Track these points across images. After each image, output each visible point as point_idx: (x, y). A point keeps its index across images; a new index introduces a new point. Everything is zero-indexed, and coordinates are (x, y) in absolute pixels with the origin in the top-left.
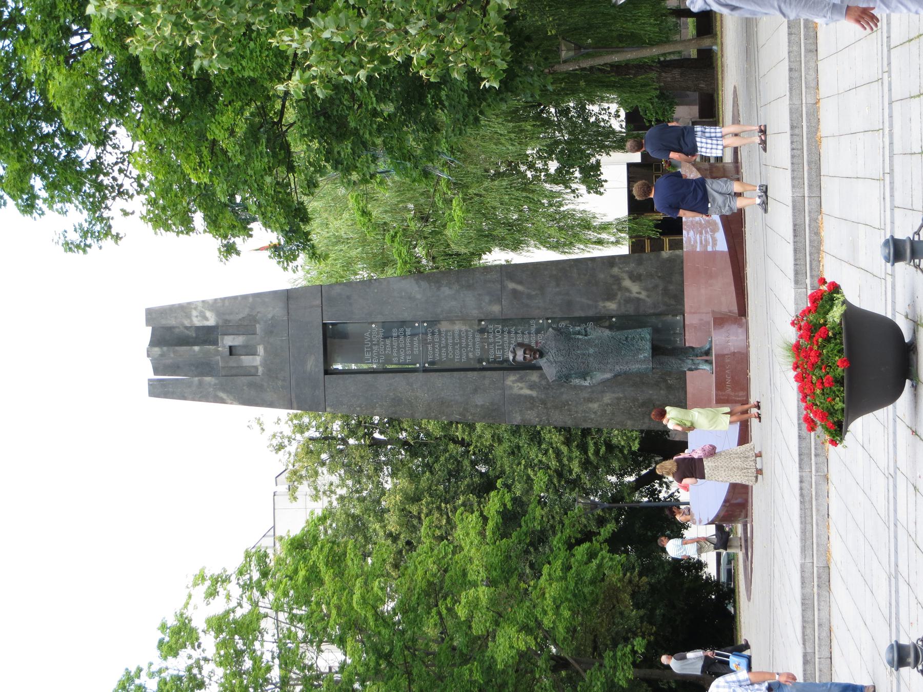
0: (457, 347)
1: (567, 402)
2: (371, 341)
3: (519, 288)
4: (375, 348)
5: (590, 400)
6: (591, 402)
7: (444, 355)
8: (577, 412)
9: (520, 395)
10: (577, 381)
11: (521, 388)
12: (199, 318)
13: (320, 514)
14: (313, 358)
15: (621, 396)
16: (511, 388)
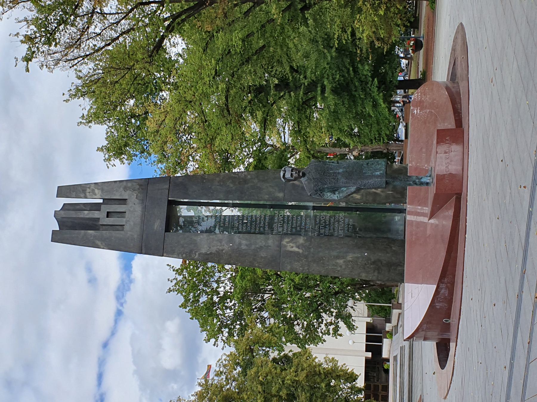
0: (254, 223)
1: (322, 258)
5: (338, 257)
6: (339, 259)
8: (328, 265)
9: (291, 252)
10: (329, 194)
11: (292, 247)
12: (91, 194)
14: (159, 221)
15: (359, 256)
16: (286, 246)
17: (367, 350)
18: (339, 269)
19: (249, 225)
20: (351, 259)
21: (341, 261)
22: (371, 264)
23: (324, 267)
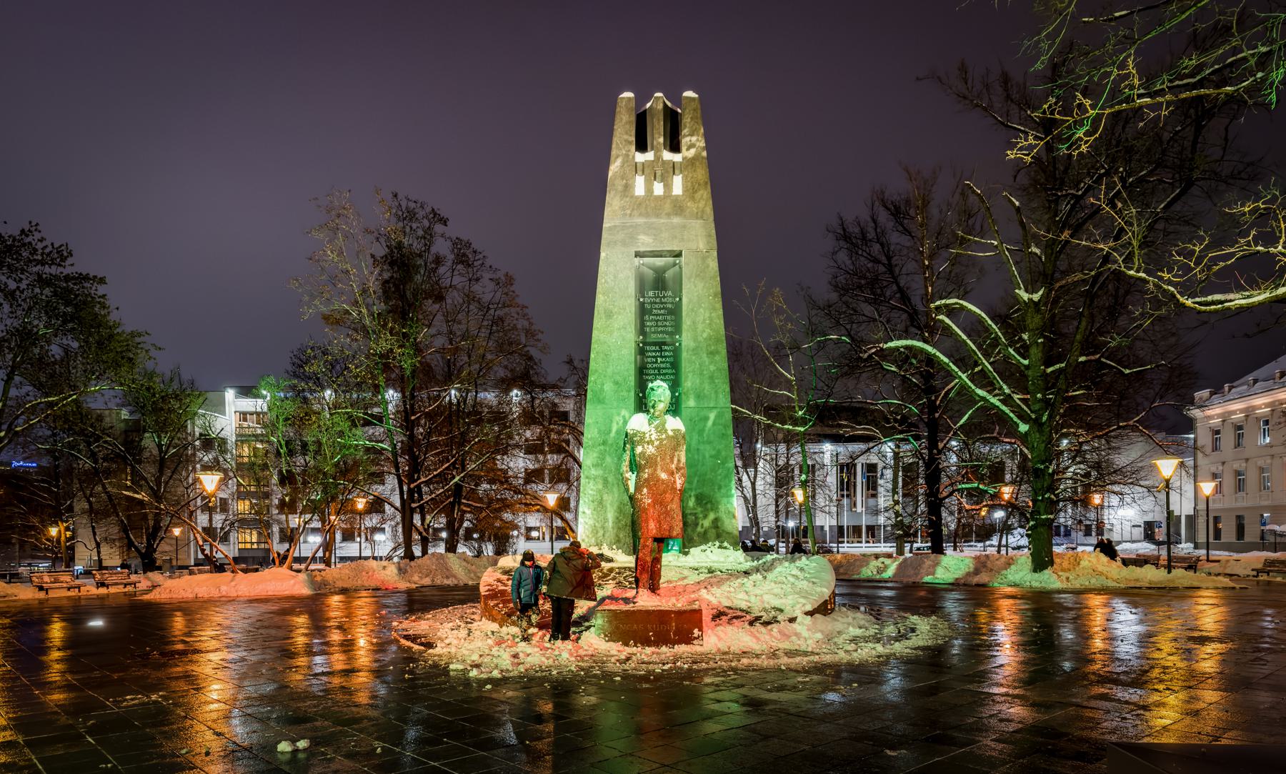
2: (664, 297)
3: (710, 423)
4: (658, 300)
7: (649, 360)
11: (618, 424)
13: (861, 617)
16: (619, 415)
19: (654, 366)
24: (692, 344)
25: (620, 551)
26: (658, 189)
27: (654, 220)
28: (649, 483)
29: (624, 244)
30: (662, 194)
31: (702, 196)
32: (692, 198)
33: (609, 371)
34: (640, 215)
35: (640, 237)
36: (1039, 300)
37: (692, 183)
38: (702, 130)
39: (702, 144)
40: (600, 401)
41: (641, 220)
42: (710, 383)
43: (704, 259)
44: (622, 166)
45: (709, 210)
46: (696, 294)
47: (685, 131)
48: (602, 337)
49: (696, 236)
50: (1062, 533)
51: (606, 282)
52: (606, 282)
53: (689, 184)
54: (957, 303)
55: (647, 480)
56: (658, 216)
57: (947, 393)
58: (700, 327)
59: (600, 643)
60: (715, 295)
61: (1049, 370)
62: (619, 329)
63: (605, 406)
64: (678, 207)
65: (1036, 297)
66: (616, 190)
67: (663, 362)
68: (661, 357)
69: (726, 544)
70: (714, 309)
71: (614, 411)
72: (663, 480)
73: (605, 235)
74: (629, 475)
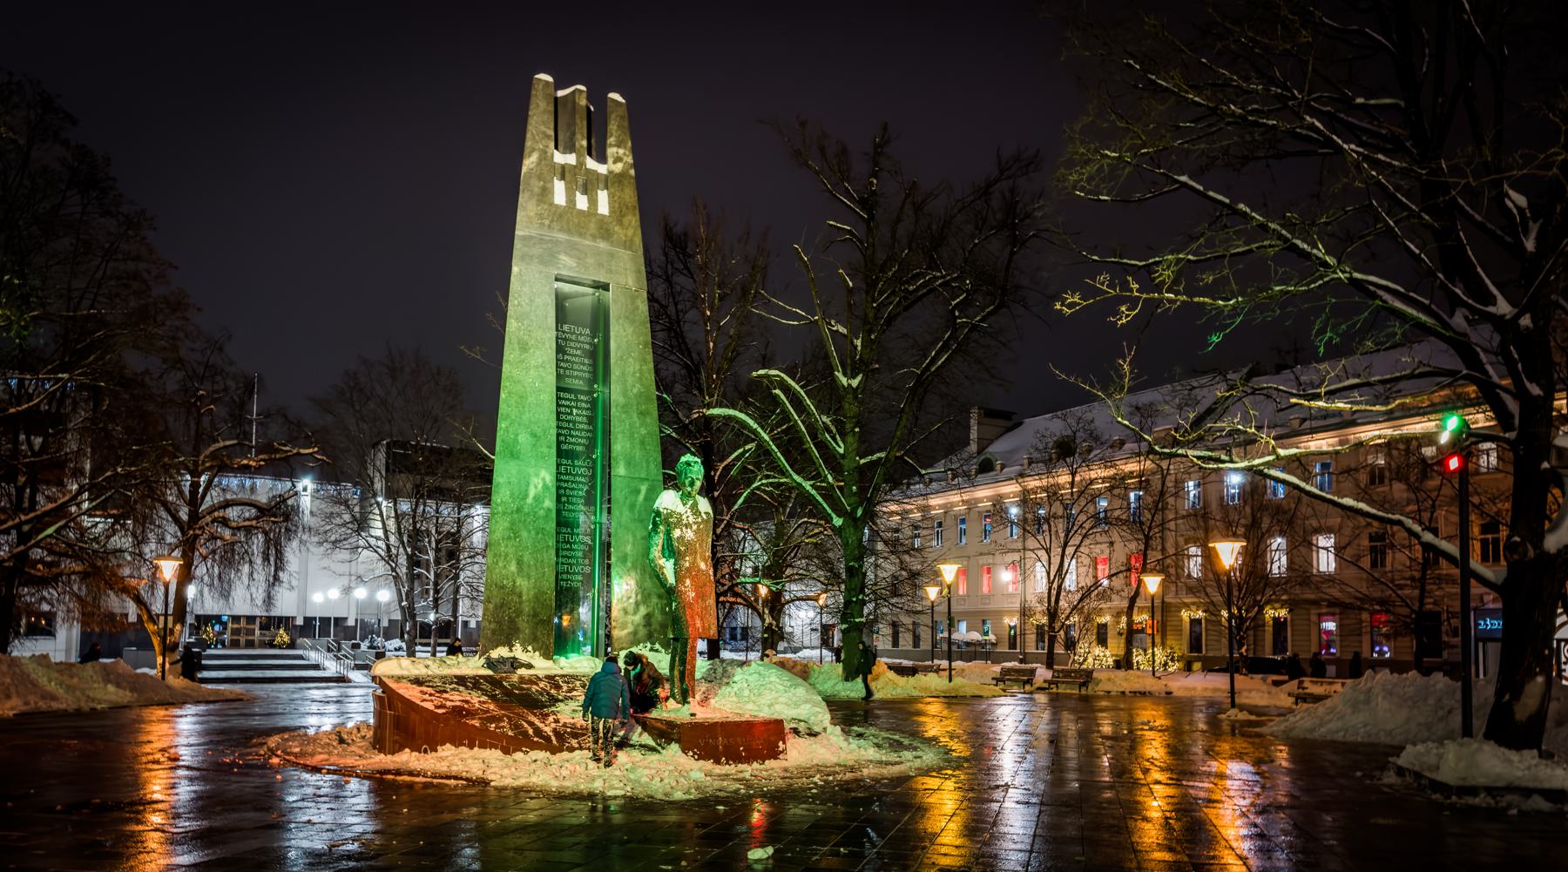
5: (520, 563)
11: (536, 487)
16: (537, 475)
17: (306, 619)
18: (500, 564)
19: (569, 417)
20: (518, 584)
21: (513, 568)
22: (510, 617)
23: (503, 539)
24: (621, 400)
25: (537, 653)
26: (582, 202)
27: (576, 239)
28: (691, 573)
29: (542, 262)
30: (586, 209)
31: (630, 222)
32: (620, 222)
33: (526, 417)
34: (560, 230)
35: (561, 257)
36: (858, 387)
37: (619, 203)
38: (630, 144)
39: (630, 160)
40: (514, 455)
41: (562, 236)
42: (641, 450)
43: (633, 299)
44: (539, 164)
45: (638, 240)
46: (625, 340)
47: (611, 140)
48: (515, 373)
49: (626, 269)
50: (739, 637)
51: (519, 304)
52: (519, 304)
53: (617, 205)
54: (778, 376)
55: (688, 569)
56: (581, 235)
57: (728, 469)
58: (630, 380)
59: (690, 762)
60: (645, 346)
61: (862, 461)
62: (537, 367)
63: (520, 463)
64: (604, 230)
65: (855, 383)
66: (532, 191)
67: (579, 415)
68: (577, 408)
69: (657, 646)
70: (644, 360)
71: (532, 471)
72: (699, 570)
73: (517, 244)
74: (662, 562)
